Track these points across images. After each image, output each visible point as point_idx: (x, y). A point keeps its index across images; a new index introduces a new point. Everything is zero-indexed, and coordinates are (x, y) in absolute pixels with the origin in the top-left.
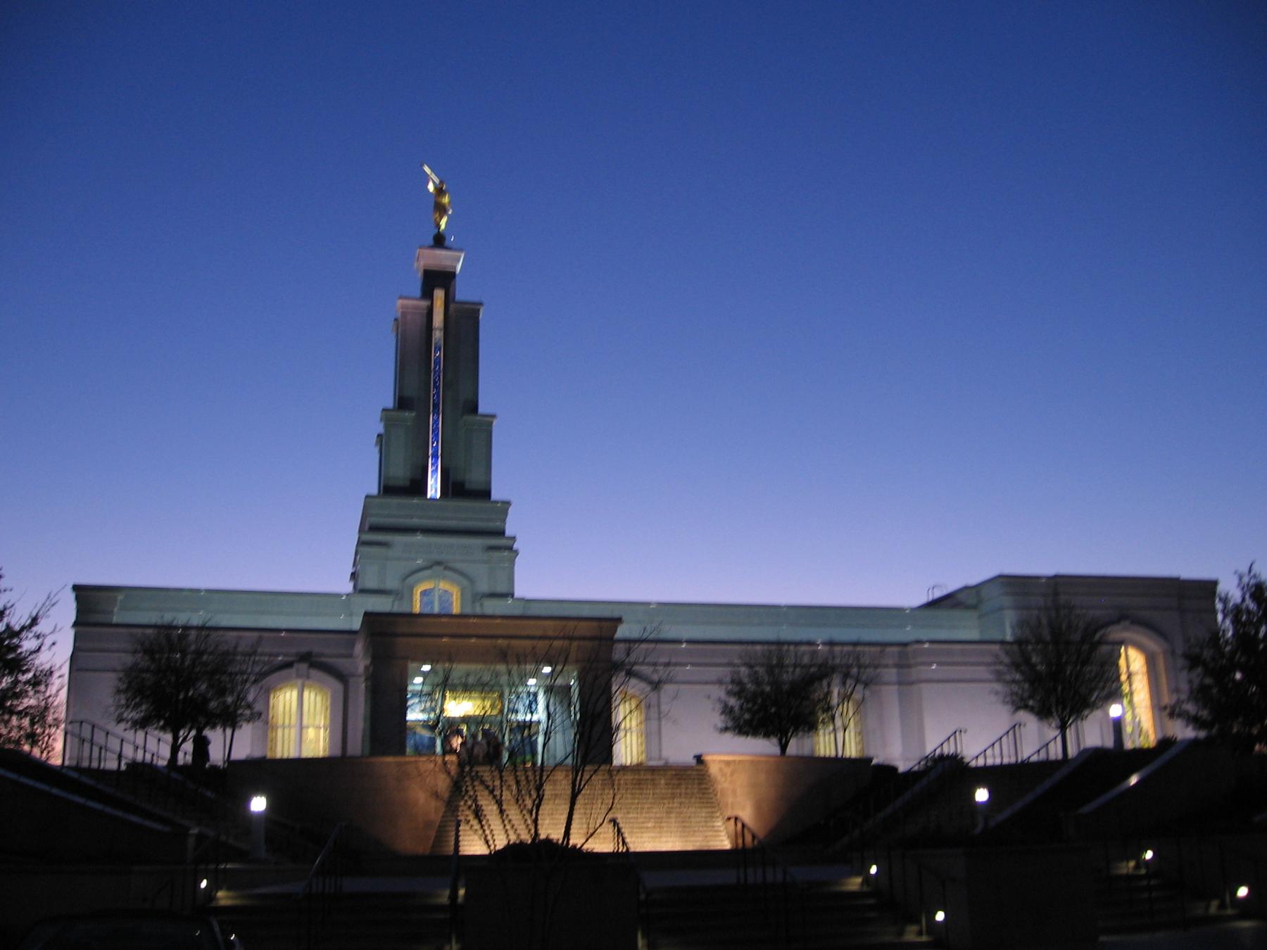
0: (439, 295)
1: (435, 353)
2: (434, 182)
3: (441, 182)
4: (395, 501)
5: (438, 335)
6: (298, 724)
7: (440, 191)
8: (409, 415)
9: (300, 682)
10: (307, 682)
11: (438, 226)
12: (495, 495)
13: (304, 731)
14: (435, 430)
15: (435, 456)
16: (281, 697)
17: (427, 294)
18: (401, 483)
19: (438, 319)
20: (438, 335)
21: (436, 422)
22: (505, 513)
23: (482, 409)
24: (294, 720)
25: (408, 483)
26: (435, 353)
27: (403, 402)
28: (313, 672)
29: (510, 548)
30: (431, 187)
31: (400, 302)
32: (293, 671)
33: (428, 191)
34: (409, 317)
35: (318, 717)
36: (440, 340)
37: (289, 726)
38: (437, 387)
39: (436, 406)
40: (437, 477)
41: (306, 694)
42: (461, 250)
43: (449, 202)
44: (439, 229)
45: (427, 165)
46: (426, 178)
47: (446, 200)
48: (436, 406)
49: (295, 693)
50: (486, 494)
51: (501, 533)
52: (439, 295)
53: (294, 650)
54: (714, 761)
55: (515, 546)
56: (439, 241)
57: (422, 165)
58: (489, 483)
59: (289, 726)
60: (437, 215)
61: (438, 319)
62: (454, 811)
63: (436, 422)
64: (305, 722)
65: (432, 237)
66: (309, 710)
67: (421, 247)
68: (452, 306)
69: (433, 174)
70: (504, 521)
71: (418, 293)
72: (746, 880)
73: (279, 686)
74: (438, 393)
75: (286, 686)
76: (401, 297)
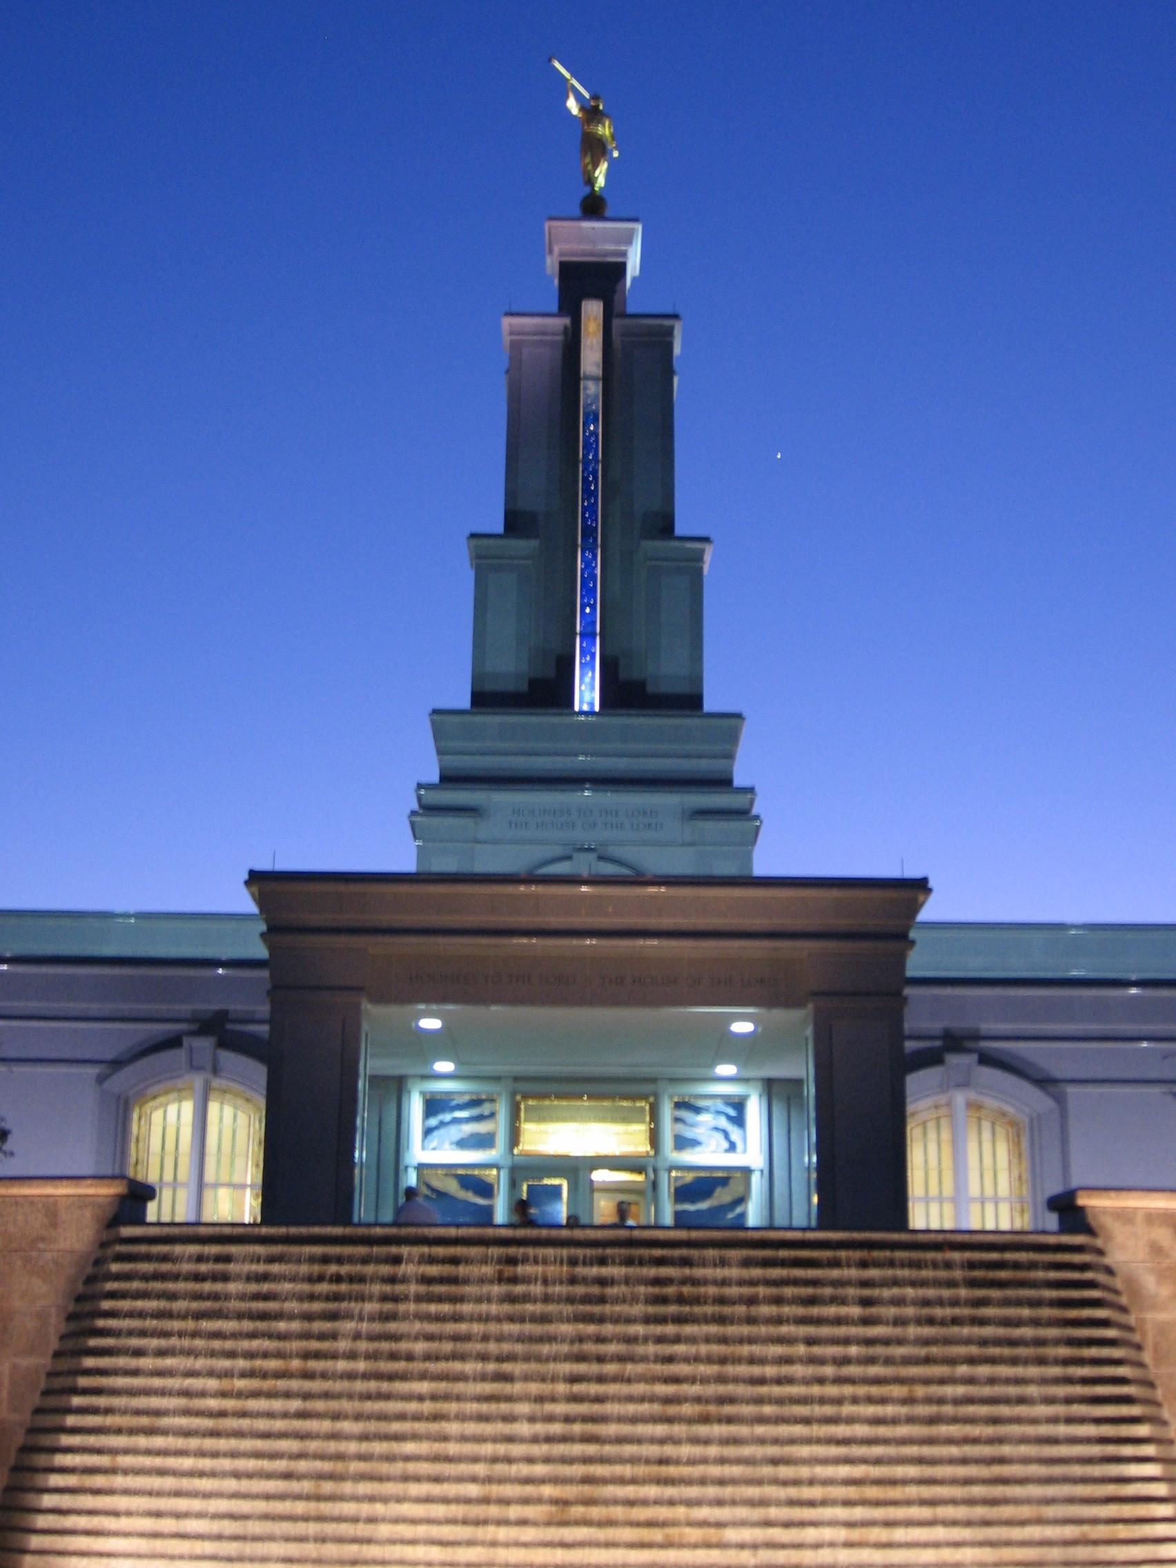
0: (592, 310)
1: (586, 424)
2: (579, 97)
3: (595, 97)
4: (493, 720)
5: (591, 390)
6: (195, 1178)
7: (592, 113)
8: (523, 546)
9: (198, 1080)
10: (216, 1083)
11: (590, 181)
12: (710, 704)
13: (208, 1194)
14: (589, 578)
15: (588, 635)
16: (157, 1116)
17: (570, 306)
18: (510, 686)
19: (591, 358)
20: (591, 390)
21: (588, 565)
22: (733, 737)
23: (682, 527)
24: (185, 1170)
25: (524, 687)
26: (586, 424)
27: (516, 523)
28: (228, 1058)
29: (743, 813)
30: (572, 105)
31: (507, 322)
32: (179, 1055)
33: (568, 111)
34: (525, 351)
35: (239, 1162)
36: (597, 396)
37: (175, 1183)
38: (589, 494)
39: (589, 532)
40: (593, 678)
41: (213, 1108)
42: (636, 220)
43: (613, 137)
44: (592, 185)
45: (558, 60)
46: (563, 89)
47: (604, 130)
48: (589, 532)
49: (188, 1108)
50: (691, 702)
51: (724, 782)
52: (592, 310)
53: (185, 1008)
54: (1126, 1216)
55: (755, 811)
56: (593, 207)
57: (550, 60)
58: (697, 679)
59: (175, 1183)
60: (588, 160)
61: (591, 358)
62: (16, 1203)
63: (588, 565)
64: (210, 1176)
65: (579, 202)
66: (219, 1146)
67: (551, 219)
68: (616, 322)
69: (573, 79)
70: (731, 756)
71: (554, 308)
72: (221, 1110)
73: (151, 1091)
74: (592, 509)
75: (167, 1092)
76: (510, 314)
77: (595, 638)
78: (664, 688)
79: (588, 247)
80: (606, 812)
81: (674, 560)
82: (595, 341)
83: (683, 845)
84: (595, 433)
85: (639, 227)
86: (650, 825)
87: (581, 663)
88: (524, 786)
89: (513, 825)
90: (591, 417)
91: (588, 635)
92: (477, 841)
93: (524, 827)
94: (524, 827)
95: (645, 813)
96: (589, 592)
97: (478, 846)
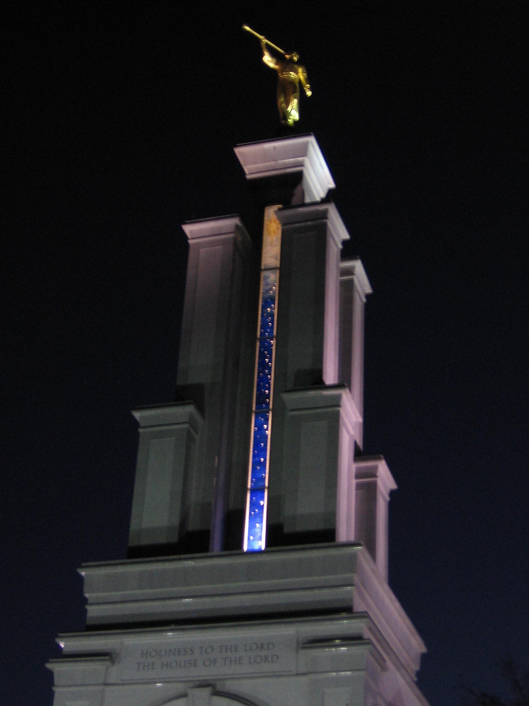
1: (264, 307)
2: (274, 53)
14: (261, 436)
18: (162, 539)
38: (264, 366)
48: (262, 399)
77: (263, 492)
78: (301, 527)
79: (271, 164)
80: (226, 648)
81: (311, 409)
82: (274, 238)
83: (297, 674)
84: (272, 315)
85: (312, 141)
86: (266, 658)
87: (250, 514)
88: (131, 621)
89: (141, 668)
90: (268, 302)
91: (257, 491)
92: (106, 684)
93: (150, 667)
94: (150, 667)
95: (262, 647)
96: (260, 451)
97: (108, 689)
